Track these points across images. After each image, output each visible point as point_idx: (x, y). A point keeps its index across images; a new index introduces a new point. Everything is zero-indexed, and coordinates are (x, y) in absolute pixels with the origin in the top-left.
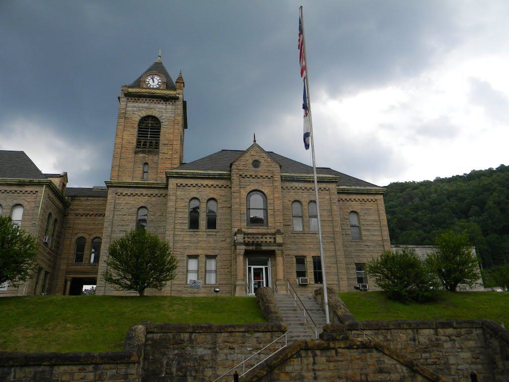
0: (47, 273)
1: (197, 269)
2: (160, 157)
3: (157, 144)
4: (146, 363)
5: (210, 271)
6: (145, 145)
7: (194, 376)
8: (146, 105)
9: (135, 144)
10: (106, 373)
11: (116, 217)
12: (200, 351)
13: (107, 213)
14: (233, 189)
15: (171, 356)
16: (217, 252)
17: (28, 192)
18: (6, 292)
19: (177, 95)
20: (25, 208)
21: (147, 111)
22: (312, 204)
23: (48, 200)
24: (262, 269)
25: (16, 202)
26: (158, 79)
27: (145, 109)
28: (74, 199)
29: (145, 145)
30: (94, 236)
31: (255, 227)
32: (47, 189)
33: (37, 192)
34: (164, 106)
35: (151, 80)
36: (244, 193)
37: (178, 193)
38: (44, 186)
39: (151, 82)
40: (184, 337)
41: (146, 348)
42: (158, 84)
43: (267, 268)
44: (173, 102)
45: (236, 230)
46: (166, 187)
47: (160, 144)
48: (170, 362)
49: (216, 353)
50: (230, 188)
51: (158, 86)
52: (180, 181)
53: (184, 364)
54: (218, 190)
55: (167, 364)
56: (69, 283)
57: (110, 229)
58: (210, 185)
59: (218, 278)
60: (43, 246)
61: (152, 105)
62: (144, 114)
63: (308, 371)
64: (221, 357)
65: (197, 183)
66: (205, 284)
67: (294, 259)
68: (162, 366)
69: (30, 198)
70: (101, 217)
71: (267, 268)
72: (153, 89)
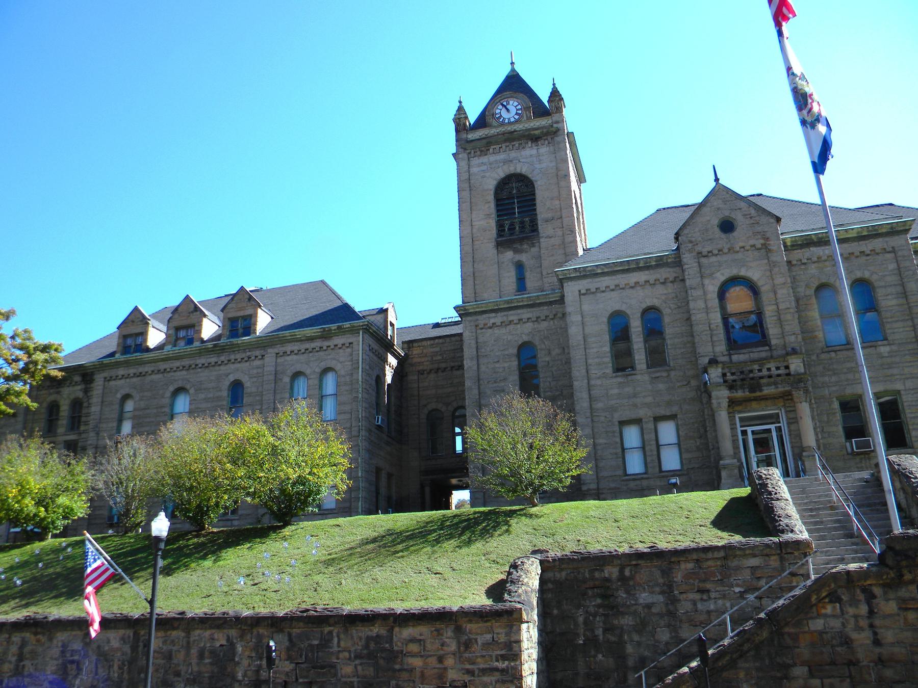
0: (390, 476)
1: (676, 442)
2: (543, 245)
3: (534, 228)
4: (549, 621)
5: (232, 524)
6: (512, 228)
7: (637, 642)
8: (502, 156)
9: (494, 231)
10: (476, 640)
11: (483, 368)
12: (644, 597)
13: (467, 363)
14: (688, 283)
15: (592, 609)
16: (675, 409)
17: (339, 346)
18: (335, 511)
19: (555, 125)
20: (339, 373)
21: (505, 167)
22: (826, 293)
23: (371, 355)
24: (769, 431)
25: (323, 365)
26: (516, 104)
27: (501, 164)
28: (413, 347)
29: (512, 228)
30: (455, 405)
31: (754, 350)
32: (366, 336)
33: (352, 343)
34: (534, 152)
35: (504, 110)
36: (712, 288)
37: (586, 307)
38: (361, 333)
39: (504, 112)
40: (611, 573)
41: (545, 596)
42: (517, 114)
43: (780, 427)
44: (549, 139)
45: (706, 360)
46: (561, 300)
47: (539, 222)
48: (591, 618)
49: (674, 601)
50: (683, 280)
51: (517, 117)
52: (584, 284)
53: (616, 622)
54: (660, 290)
55: (586, 623)
56: (427, 490)
57: (476, 392)
58: (652, 282)
59: (684, 456)
60: (377, 431)
61: (513, 154)
62: (501, 173)
63: (859, 629)
64: (684, 607)
65: (617, 282)
66: (661, 471)
67: (836, 405)
68: (576, 624)
69: (343, 354)
70: (459, 373)
71: (780, 427)
72: (510, 123)
